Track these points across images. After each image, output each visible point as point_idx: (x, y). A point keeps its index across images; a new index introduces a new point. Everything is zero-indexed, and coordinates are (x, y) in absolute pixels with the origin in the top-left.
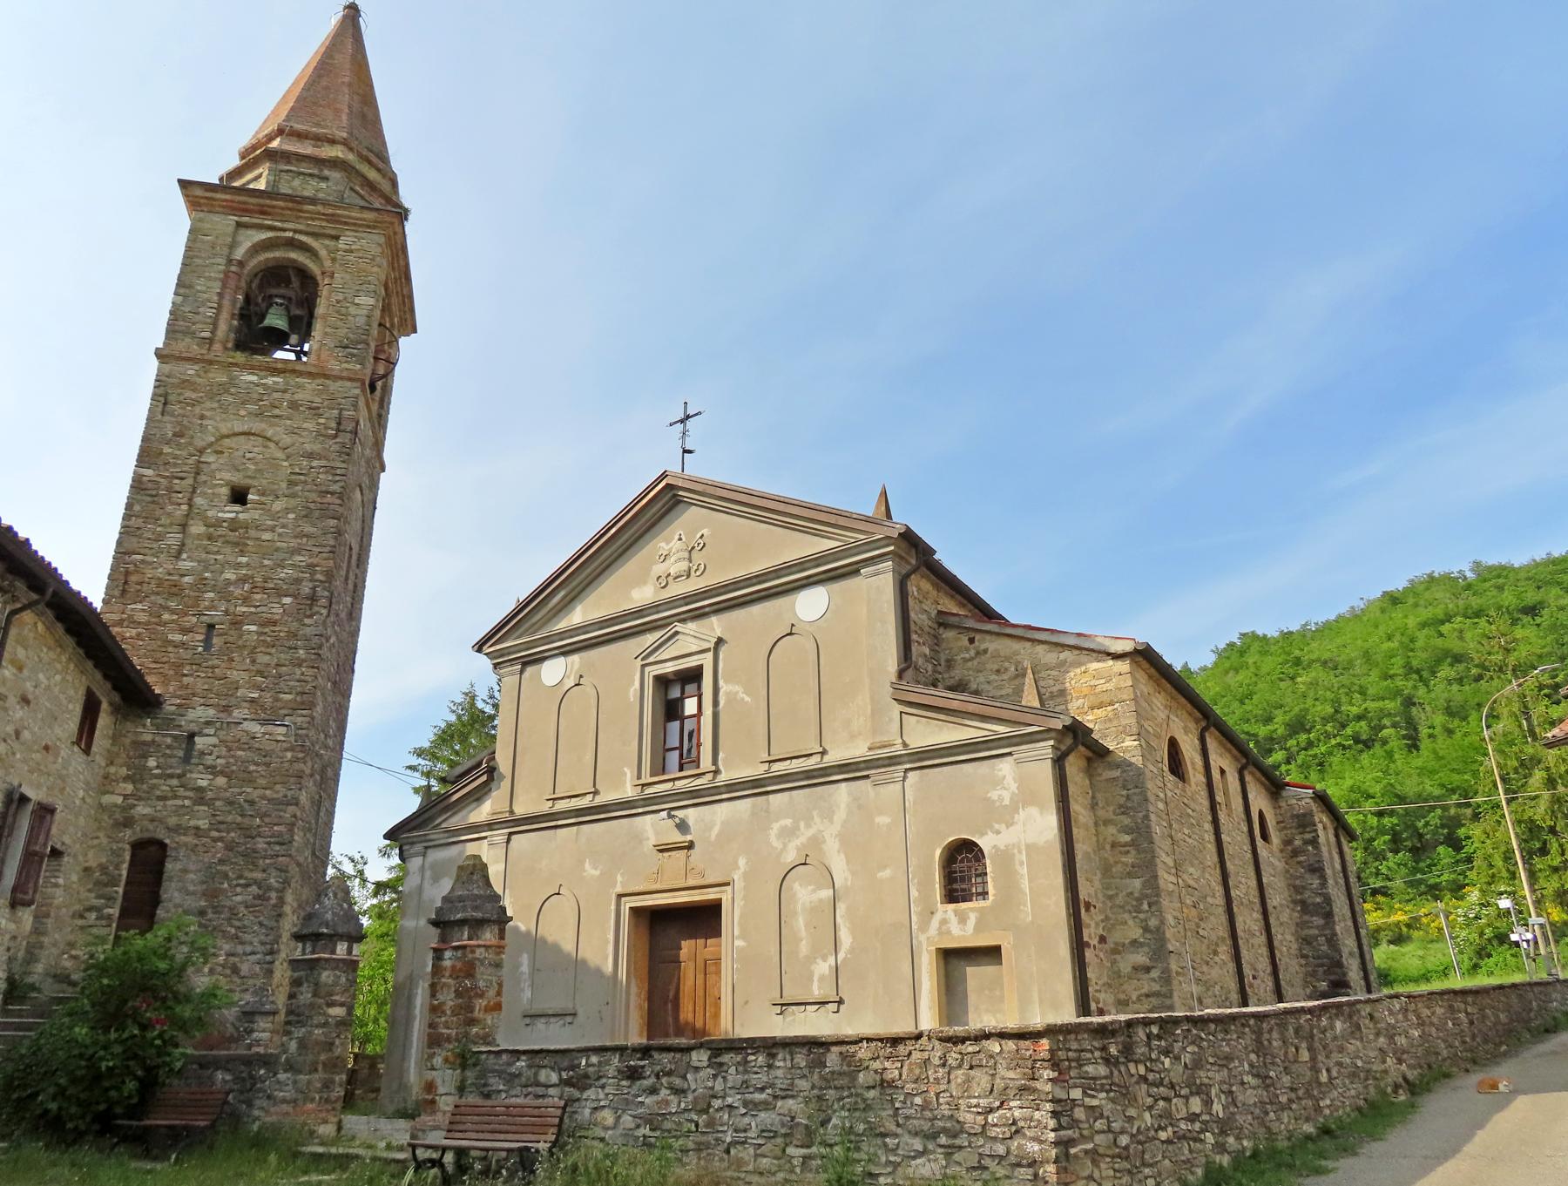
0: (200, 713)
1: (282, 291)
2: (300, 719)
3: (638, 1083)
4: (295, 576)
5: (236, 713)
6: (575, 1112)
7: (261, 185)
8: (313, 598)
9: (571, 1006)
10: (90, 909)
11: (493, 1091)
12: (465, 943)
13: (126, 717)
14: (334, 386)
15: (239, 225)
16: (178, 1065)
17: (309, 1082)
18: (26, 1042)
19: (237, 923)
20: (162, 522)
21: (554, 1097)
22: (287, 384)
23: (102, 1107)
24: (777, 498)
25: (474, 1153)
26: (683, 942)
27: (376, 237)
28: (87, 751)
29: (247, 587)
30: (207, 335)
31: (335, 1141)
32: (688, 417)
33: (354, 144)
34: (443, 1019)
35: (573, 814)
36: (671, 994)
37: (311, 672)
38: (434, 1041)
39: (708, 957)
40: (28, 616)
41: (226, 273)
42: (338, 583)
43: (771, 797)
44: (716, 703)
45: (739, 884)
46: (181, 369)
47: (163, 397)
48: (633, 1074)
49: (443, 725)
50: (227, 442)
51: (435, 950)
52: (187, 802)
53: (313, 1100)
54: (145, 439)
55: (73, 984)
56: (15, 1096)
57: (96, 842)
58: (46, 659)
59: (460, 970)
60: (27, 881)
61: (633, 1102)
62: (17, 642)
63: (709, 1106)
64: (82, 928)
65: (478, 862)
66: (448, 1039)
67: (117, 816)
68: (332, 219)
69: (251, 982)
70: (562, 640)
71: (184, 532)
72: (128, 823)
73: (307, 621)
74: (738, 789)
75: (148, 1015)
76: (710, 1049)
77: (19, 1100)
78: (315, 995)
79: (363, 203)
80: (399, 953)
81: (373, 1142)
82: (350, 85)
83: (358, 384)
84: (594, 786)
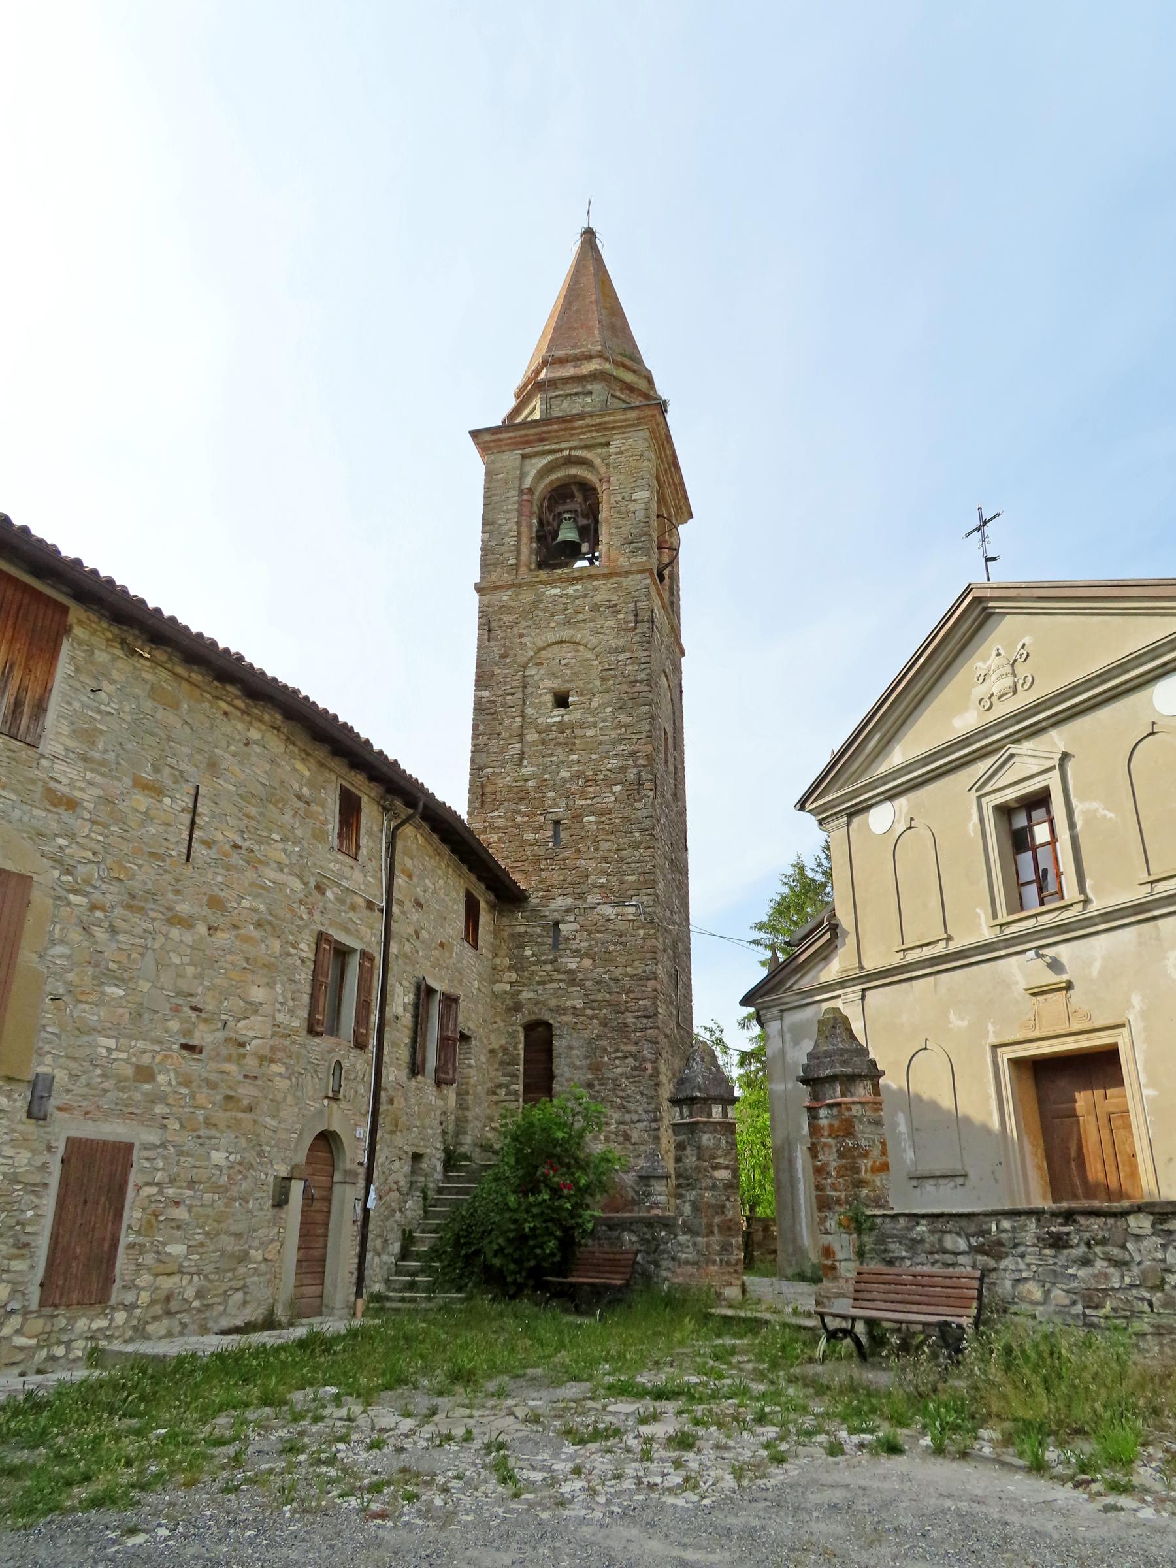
0: (560, 903)
1: (568, 507)
2: (645, 898)
3: (1065, 1252)
4: (620, 764)
5: (590, 899)
6: (994, 1284)
7: (537, 416)
8: (639, 783)
9: (959, 1166)
10: (500, 1086)
11: (897, 1258)
12: (839, 1100)
13: (501, 913)
14: (626, 582)
15: (524, 457)
16: (590, 1226)
17: (708, 1245)
18: (465, 1205)
19: (621, 1094)
20: (503, 736)
21: (966, 1267)
22: (585, 589)
23: (532, 1263)
24: (1109, 583)
25: (886, 1325)
26: (1079, 1096)
27: (641, 434)
28: (475, 946)
29: (581, 782)
30: (513, 561)
31: (742, 1305)
32: (985, 523)
33: (609, 355)
34: (829, 1181)
35: (927, 963)
36: (1073, 1154)
37: (648, 852)
38: (824, 1204)
39: (1112, 1110)
40: (408, 830)
41: (520, 503)
42: (660, 766)
43: (1160, 922)
44: (1072, 825)
45: (1137, 1025)
46: (497, 597)
47: (487, 627)
48: (1058, 1243)
49: (778, 898)
50: (543, 654)
51: (809, 1109)
52: (562, 985)
53: (714, 1262)
54: (479, 666)
55: (496, 1153)
56: (463, 1252)
57: (495, 1026)
58: (429, 866)
59: (839, 1129)
60: (446, 1062)
61: (1063, 1274)
62: (405, 853)
63: (1163, 1282)
64: (496, 1103)
65: (838, 1015)
66: (838, 1201)
67: (508, 1002)
68: (601, 427)
69: (642, 1148)
70: (885, 784)
71: (521, 741)
72: (517, 1007)
73: (637, 805)
74: (1114, 918)
75: (556, 1179)
76: (1152, 1214)
77: (467, 1256)
78: (699, 1159)
79: (624, 406)
80: (772, 1118)
81: (780, 1306)
82: (597, 302)
83: (648, 575)
84: (946, 931)
